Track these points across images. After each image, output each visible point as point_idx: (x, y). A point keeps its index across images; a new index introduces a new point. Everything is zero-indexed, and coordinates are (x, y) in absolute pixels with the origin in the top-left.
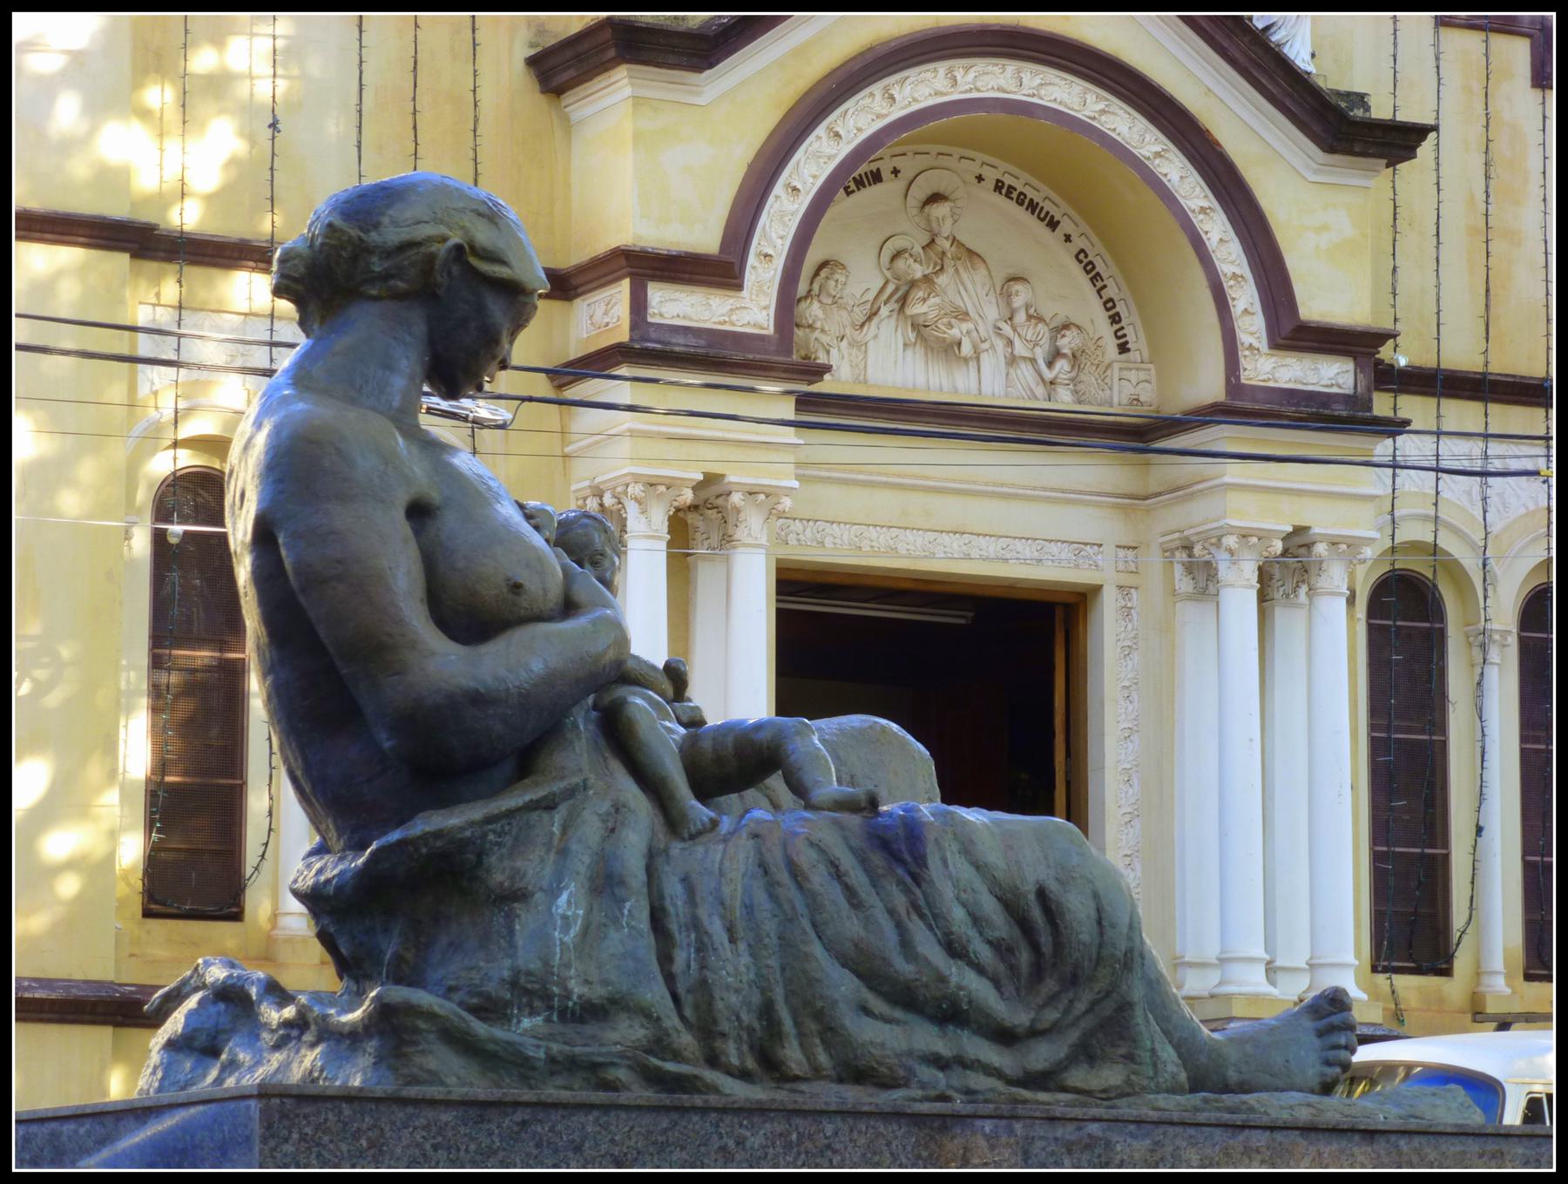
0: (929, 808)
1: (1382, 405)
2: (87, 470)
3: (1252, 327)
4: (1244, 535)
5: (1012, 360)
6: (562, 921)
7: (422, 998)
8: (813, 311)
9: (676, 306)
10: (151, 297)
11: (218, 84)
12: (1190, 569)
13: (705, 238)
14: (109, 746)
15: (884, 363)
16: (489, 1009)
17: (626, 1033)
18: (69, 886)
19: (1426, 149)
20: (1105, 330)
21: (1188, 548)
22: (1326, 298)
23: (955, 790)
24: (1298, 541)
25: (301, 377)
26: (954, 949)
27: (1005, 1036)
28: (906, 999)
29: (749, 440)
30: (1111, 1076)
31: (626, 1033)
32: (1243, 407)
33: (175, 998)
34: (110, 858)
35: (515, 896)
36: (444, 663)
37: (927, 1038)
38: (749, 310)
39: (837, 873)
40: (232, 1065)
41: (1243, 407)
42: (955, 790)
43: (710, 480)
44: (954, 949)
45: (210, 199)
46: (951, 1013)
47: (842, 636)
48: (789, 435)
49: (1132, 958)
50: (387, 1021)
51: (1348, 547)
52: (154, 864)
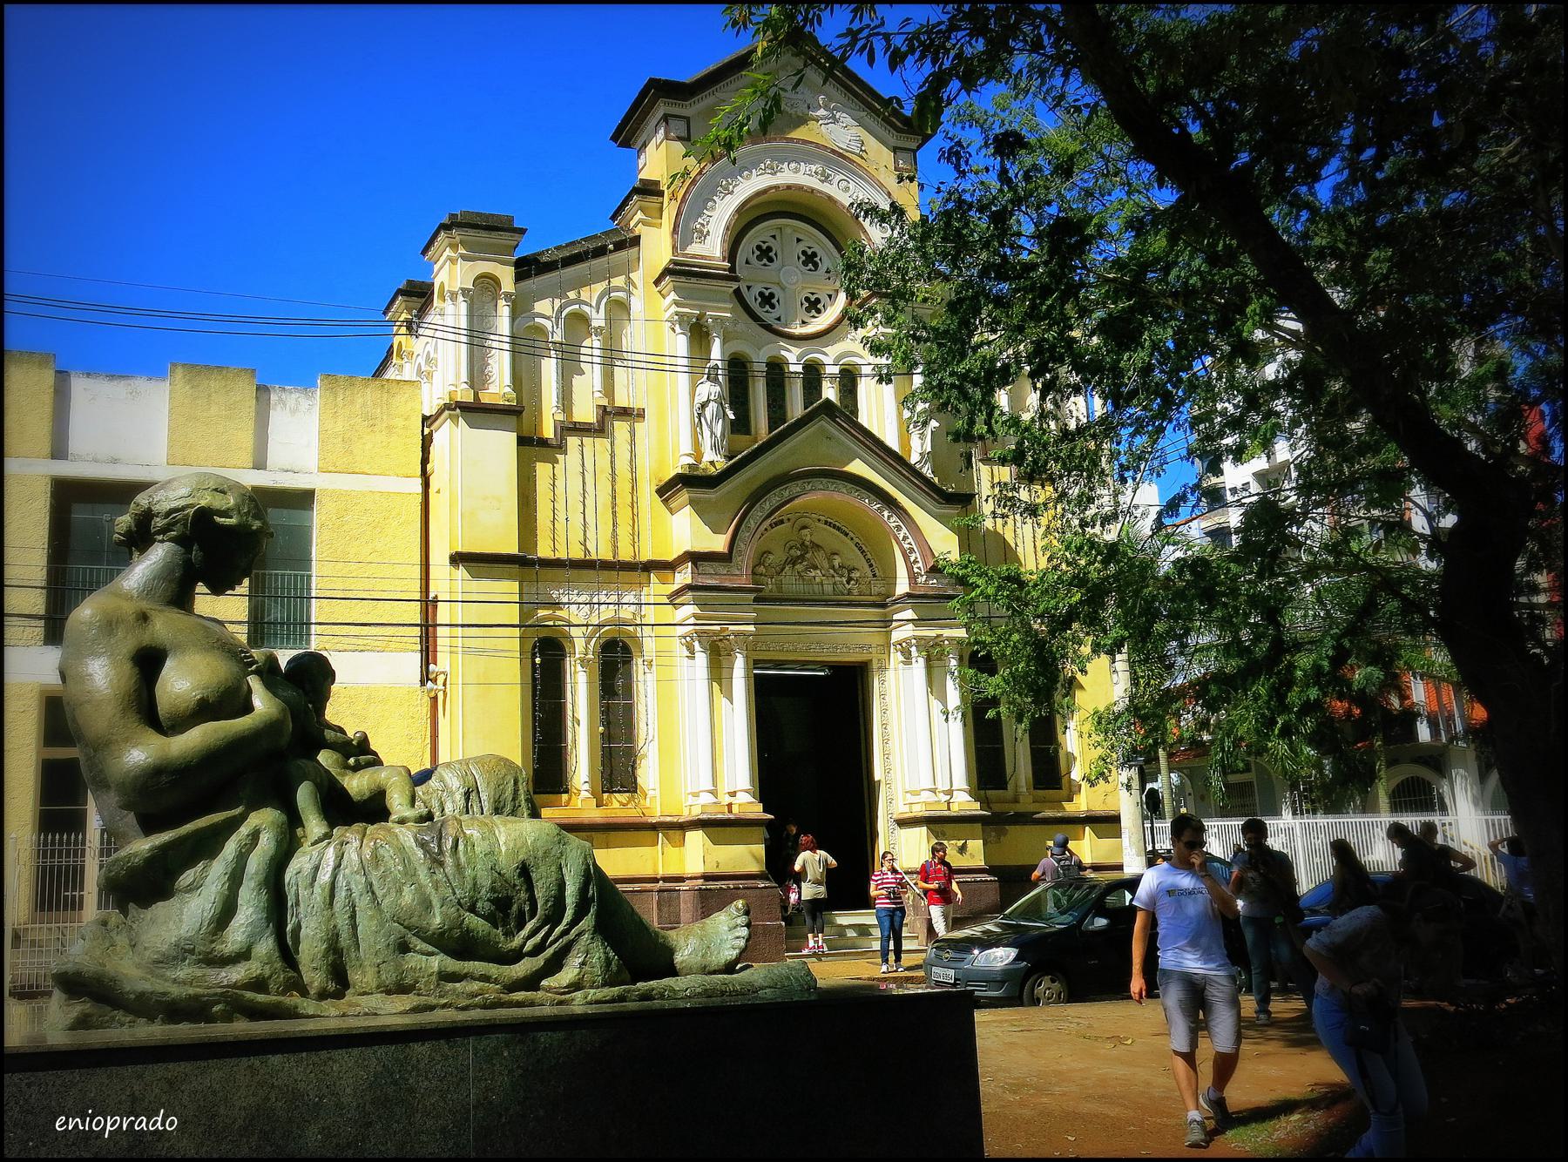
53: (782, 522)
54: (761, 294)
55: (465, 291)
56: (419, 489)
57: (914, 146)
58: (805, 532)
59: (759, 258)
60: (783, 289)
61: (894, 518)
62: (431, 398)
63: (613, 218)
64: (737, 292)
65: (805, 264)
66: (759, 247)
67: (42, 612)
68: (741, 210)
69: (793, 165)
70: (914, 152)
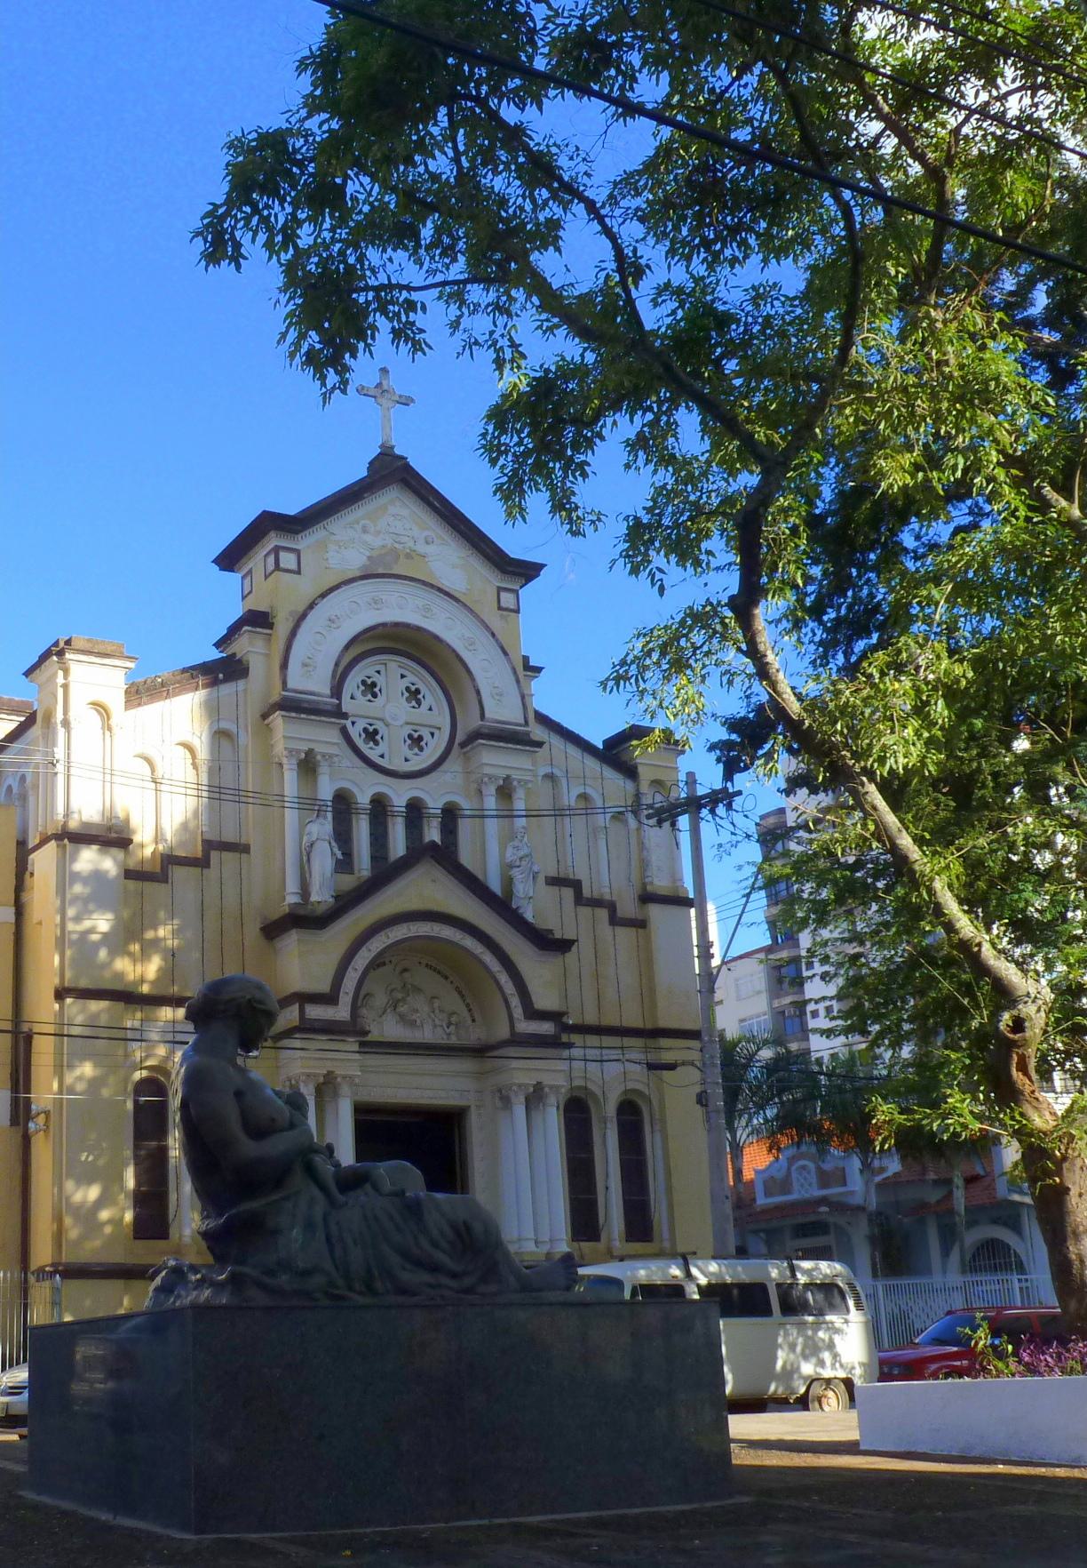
0: (423, 1194)
1: (565, 1038)
2: (111, 1080)
3: (518, 1012)
4: (520, 1086)
5: (435, 1026)
6: (295, 1236)
7: (246, 1270)
8: (364, 1011)
9: (315, 1012)
10: (132, 1020)
11: (156, 943)
12: (501, 1098)
13: (324, 987)
14: (121, 1179)
15: (389, 1029)
16: (270, 1273)
17: (318, 1281)
18: (108, 1230)
19: (574, 948)
20: (466, 1013)
21: (500, 1091)
22: (545, 999)
23: (432, 1186)
24: (539, 1087)
25: (196, 1047)
26: (435, 1245)
27: (454, 1276)
28: (419, 1263)
29: (345, 1060)
30: (493, 1288)
31: (318, 1281)
32: (517, 1040)
33: (157, 1273)
34: (122, 1218)
35: (275, 1232)
36: (249, 1148)
37: (425, 1277)
38: (341, 1012)
39: (391, 1218)
40: (179, 1296)
41: (517, 1040)
42: (432, 1186)
43: (330, 1073)
44: (435, 1245)
45: (152, 983)
46: (434, 1268)
47: (384, 1129)
48: (357, 1056)
49: (499, 1244)
50: (235, 1280)
51: (555, 1088)
52: (137, 1219)
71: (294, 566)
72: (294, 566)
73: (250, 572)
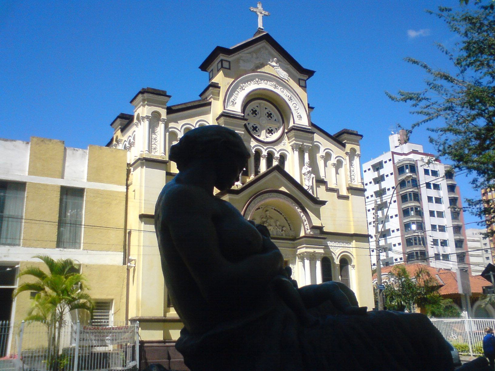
53: (259, 208)
54: (253, 126)
55: (147, 117)
56: (125, 190)
57: (305, 78)
58: (268, 212)
59: (252, 114)
60: (261, 125)
61: (304, 217)
62: (132, 156)
63: (200, 95)
64: (245, 125)
65: (268, 117)
66: (252, 110)
67: (172, 368)
68: (248, 95)
69: (265, 82)
70: (306, 81)
71: (228, 67)
72: (228, 67)
73: (212, 70)
